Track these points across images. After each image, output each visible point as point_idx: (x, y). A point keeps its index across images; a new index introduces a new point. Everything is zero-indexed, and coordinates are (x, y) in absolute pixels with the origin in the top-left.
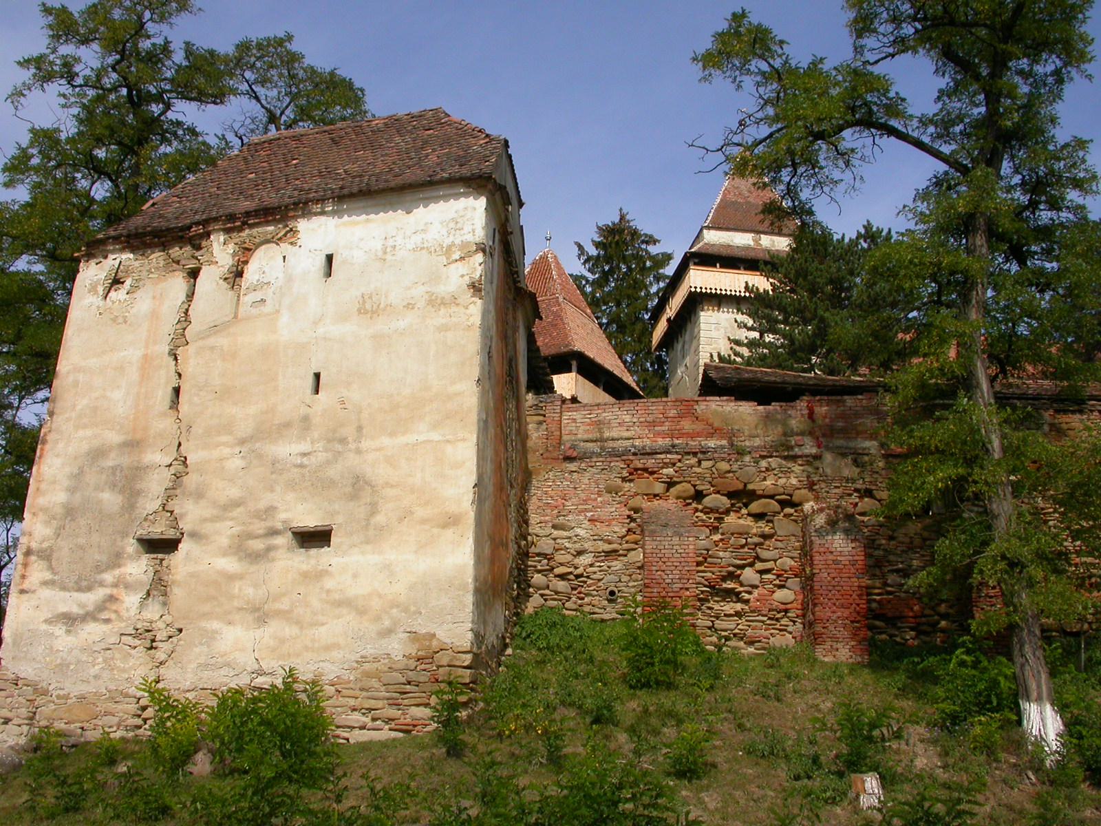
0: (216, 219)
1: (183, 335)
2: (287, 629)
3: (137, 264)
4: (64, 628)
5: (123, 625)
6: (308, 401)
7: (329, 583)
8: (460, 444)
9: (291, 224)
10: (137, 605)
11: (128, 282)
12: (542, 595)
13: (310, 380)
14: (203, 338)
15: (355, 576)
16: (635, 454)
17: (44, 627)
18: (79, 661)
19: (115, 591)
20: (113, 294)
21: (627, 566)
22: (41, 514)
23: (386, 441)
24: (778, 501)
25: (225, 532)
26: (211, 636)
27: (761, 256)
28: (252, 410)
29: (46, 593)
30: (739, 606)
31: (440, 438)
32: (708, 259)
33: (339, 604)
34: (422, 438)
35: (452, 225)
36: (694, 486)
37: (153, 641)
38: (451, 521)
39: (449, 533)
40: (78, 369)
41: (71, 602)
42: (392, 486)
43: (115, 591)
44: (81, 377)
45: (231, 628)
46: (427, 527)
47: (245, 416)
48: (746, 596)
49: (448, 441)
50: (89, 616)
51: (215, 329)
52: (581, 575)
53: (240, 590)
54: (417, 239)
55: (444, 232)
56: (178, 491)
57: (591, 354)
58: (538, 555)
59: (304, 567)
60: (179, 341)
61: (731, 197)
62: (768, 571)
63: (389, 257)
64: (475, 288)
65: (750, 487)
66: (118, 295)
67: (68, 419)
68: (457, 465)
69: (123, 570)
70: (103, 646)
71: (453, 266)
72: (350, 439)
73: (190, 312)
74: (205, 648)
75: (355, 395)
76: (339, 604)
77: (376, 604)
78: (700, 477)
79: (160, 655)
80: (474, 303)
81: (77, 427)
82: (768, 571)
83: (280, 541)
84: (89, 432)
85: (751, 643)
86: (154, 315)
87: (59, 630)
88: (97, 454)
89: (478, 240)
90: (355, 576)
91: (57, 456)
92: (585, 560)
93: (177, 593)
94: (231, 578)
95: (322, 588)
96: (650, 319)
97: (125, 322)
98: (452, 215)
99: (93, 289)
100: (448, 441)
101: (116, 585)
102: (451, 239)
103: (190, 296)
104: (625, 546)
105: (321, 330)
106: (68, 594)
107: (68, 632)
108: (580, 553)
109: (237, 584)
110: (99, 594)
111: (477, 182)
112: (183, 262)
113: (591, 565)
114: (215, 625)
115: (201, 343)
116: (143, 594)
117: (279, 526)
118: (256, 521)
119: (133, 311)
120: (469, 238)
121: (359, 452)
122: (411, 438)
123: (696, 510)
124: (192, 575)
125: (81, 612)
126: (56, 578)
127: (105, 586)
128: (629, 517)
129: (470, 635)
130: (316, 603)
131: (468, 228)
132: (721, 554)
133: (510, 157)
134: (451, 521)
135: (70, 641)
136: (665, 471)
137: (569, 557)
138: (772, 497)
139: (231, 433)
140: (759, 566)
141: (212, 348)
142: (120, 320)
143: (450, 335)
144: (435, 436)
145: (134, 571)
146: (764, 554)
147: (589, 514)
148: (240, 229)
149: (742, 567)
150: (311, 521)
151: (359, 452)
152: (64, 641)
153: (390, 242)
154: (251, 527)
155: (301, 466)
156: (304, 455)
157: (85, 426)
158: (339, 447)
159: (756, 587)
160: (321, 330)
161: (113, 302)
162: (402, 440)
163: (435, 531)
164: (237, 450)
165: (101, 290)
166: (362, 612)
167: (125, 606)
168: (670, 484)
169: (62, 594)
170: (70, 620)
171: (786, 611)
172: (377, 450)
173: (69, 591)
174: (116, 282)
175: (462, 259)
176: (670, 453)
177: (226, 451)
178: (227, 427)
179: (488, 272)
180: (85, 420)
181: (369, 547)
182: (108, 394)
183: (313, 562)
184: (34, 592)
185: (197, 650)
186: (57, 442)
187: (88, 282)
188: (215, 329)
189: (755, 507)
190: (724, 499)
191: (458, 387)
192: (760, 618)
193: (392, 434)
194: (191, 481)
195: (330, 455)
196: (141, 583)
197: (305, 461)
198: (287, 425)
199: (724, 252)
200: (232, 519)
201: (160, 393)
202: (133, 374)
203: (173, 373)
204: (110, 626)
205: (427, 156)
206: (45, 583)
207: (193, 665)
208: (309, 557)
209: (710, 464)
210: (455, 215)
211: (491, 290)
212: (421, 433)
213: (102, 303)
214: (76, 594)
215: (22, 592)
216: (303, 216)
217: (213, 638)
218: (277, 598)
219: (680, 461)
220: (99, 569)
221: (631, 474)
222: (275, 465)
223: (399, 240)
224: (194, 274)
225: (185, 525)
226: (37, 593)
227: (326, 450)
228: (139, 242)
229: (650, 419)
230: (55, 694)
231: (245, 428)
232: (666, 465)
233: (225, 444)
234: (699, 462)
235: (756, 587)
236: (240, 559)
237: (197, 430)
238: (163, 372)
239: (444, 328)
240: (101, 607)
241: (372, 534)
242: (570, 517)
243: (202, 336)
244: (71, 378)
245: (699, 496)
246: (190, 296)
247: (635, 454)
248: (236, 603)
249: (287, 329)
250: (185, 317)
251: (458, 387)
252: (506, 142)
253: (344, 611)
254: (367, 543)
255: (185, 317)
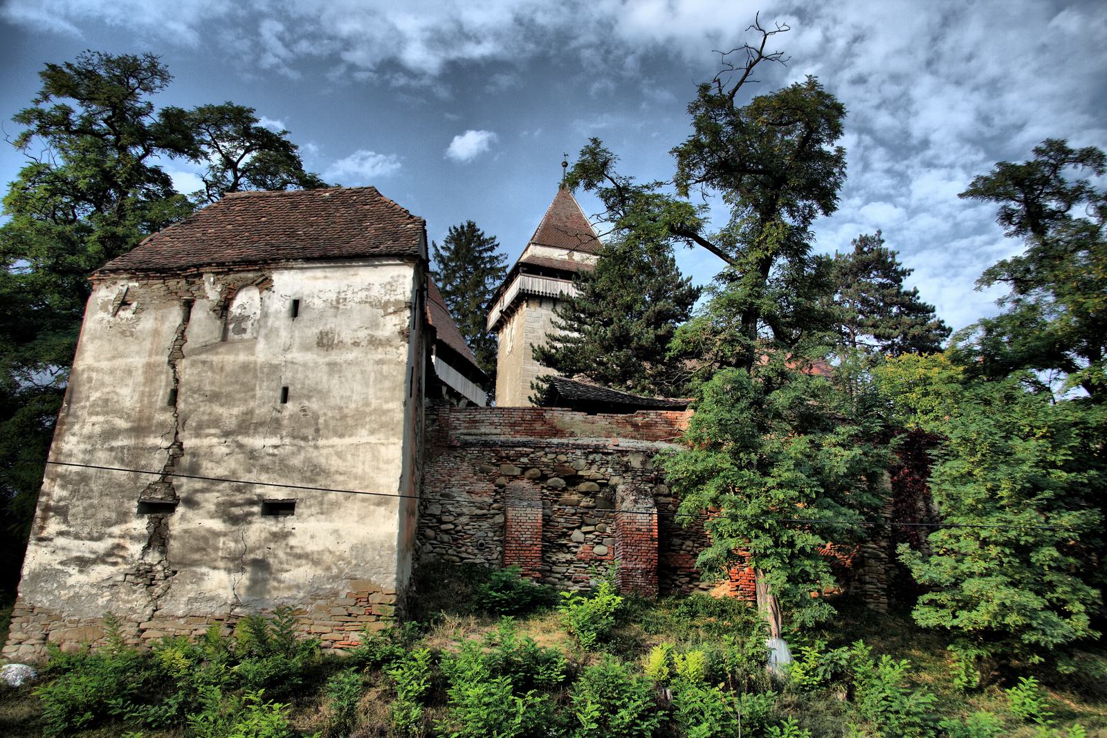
0: (209, 264)
1: (180, 349)
2: (260, 574)
3: (142, 291)
4: (77, 568)
5: (128, 567)
6: (278, 408)
7: (292, 541)
8: (391, 447)
9: (267, 273)
10: (140, 552)
11: (134, 305)
12: (432, 544)
13: (279, 393)
14: (196, 354)
15: (312, 537)
16: (501, 446)
17: (60, 567)
18: (90, 594)
19: (122, 541)
20: (121, 313)
21: (492, 526)
22: (58, 480)
23: (335, 441)
24: (599, 484)
25: (211, 500)
26: (200, 579)
27: (574, 269)
28: (235, 411)
29: (61, 541)
30: (569, 556)
31: (377, 441)
32: (532, 268)
33: (299, 557)
34: (364, 440)
35: (388, 287)
36: (542, 471)
37: (153, 579)
38: (383, 499)
39: (382, 509)
40: (91, 369)
41: (84, 548)
42: (341, 474)
43: (122, 541)
44: (94, 375)
45: (216, 572)
46: (366, 504)
47: (229, 414)
48: (575, 550)
49: (383, 444)
50: (102, 559)
51: (207, 348)
52: (460, 531)
53: (224, 543)
54: (362, 295)
55: (383, 291)
56: (175, 468)
57: (447, 341)
58: (430, 515)
59: (274, 529)
60: (176, 354)
61: (554, 221)
62: (590, 532)
63: (341, 306)
64: (404, 334)
65: (580, 473)
66: (126, 314)
67: (84, 407)
68: (388, 462)
69: (129, 525)
70: (111, 582)
71: (388, 318)
72: (310, 438)
73: (186, 333)
74: (195, 586)
75: (314, 405)
76: (299, 557)
77: (327, 558)
78: (547, 466)
79: (158, 590)
80: (403, 346)
81: (91, 414)
82: (590, 532)
83: (256, 509)
84: (101, 419)
85: (576, 582)
86: (156, 333)
87: (73, 570)
88: (110, 434)
89: (407, 300)
90: (312, 537)
91: (74, 435)
92: (464, 520)
93: (174, 545)
94: (217, 535)
95: (287, 545)
96: (486, 308)
97: (132, 336)
98: (388, 279)
99: (104, 307)
100: (383, 444)
101: (122, 537)
102: (388, 297)
103: (187, 319)
104: (492, 512)
105: (289, 356)
106: (81, 542)
107: (81, 571)
108: (460, 515)
109: (222, 539)
110: (107, 543)
111: (403, 257)
112: (179, 294)
113: (467, 525)
114: (204, 570)
115: (194, 358)
116: (143, 544)
117: (255, 498)
118: (237, 494)
119: (139, 328)
120: (401, 297)
121: (316, 447)
122: (354, 440)
123: (543, 488)
124: (186, 531)
125: (93, 556)
126: (72, 529)
127: (114, 537)
128: (495, 491)
129: (395, 584)
130: (281, 554)
131: (400, 291)
132: (559, 520)
133: (425, 231)
134: (383, 499)
135: (83, 578)
136: (522, 460)
137: (452, 518)
138: (594, 481)
139: (218, 427)
140: (585, 529)
141: (204, 362)
142: (128, 334)
143: (385, 368)
144: (373, 439)
145: (138, 527)
146: (588, 521)
147: (467, 488)
148: (227, 273)
149: (573, 529)
150: (279, 495)
151: (316, 447)
152: (75, 577)
153: (343, 295)
154: (233, 498)
155: (274, 455)
156: (276, 447)
157: (97, 414)
158: (302, 443)
159: (582, 543)
160: (289, 356)
161: (122, 319)
162: (347, 441)
163: (372, 507)
164: (223, 440)
165: (111, 308)
166: (316, 563)
167: (129, 552)
168: (525, 469)
169: (77, 542)
170: (83, 563)
171: (602, 561)
172: (329, 447)
173: (82, 540)
174: (124, 303)
175: (395, 312)
176: (525, 446)
177: (215, 440)
178: (216, 422)
179: (413, 323)
180: (98, 409)
181: (323, 517)
182: (118, 390)
183: (280, 525)
184: (51, 540)
185: (189, 587)
186: (73, 424)
187: (100, 301)
188: (207, 348)
189: (583, 487)
190: (562, 481)
191: (391, 406)
192: (583, 565)
193: (341, 436)
194: (185, 460)
195: (295, 449)
196: (144, 536)
197: (276, 451)
198: (262, 424)
199: (547, 264)
200: (219, 491)
201: (161, 392)
202: (139, 377)
203: (171, 378)
204: (117, 568)
205: (366, 228)
206: (61, 534)
207: (185, 599)
208: (278, 521)
209: (554, 456)
210: (391, 280)
211: (414, 334)
212: (362, 436)
213: (112, 319)
214: (88, 543)
215: (41, 540)
216: (277, 269)
217: (202, 579)
218: (252, 550)
219: (532, 453)
220: (108, 523)
221: (498, 461)
222: (252, 455)
223: (349, 295)
224: (188, 305)
225: (181, 494)
226: (55, 541)
227: (292, 445)
228: (143, 272)
229: (512, 421)
230: (67, 619)
231: (231, 423)
232: (523, 455)
233: (214, 435)
234: (546, 454)
235: (582, 543)
236: (224, 521)
237: (192, 422)
238: (163, 377)
239: (380, 362)
240: (110, 553)
241: (326, 510)
242: (454, 489)
243: (195, 352)
244: (85, 376)
245: (544, 478)
246: (187, 319)
247: (501, 446)
248: (220, 554)
249: (262, 353)
250: (182, 335)
251: (391, 406)
252: (425, 222)
253: (304, 562)
254: (322, 513)
255: (182, 335)
